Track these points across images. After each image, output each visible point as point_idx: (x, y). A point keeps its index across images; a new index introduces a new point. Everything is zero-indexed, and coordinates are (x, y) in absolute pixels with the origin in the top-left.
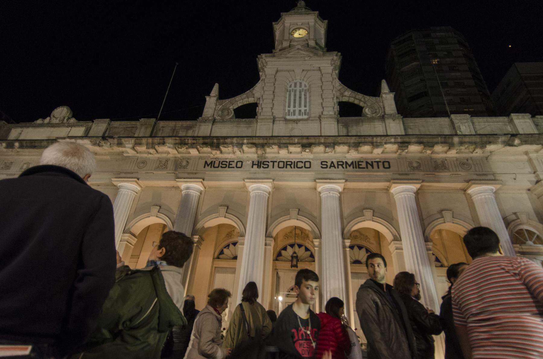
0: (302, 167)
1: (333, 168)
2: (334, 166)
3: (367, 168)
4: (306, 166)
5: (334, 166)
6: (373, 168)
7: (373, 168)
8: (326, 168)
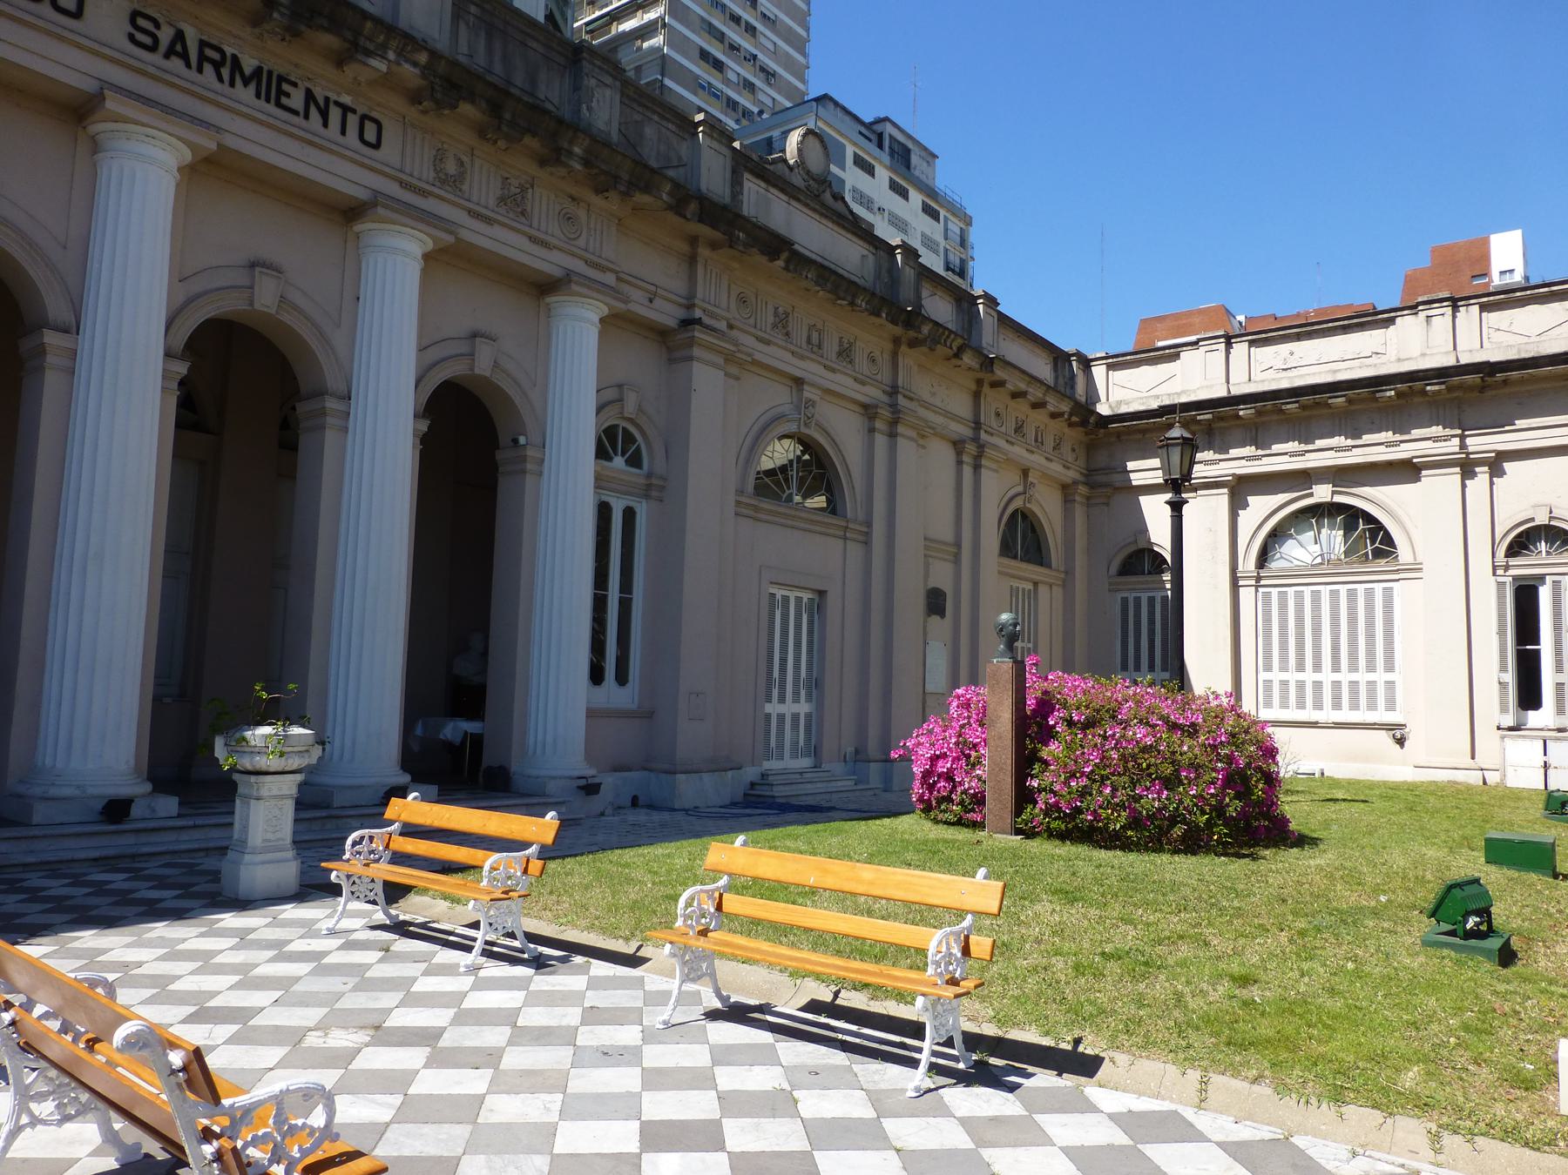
1: (176, 64)
2: (185, 57)
5: (185, 57)
6: (325, 125)
7: (325, 125)
8: (152, 49)
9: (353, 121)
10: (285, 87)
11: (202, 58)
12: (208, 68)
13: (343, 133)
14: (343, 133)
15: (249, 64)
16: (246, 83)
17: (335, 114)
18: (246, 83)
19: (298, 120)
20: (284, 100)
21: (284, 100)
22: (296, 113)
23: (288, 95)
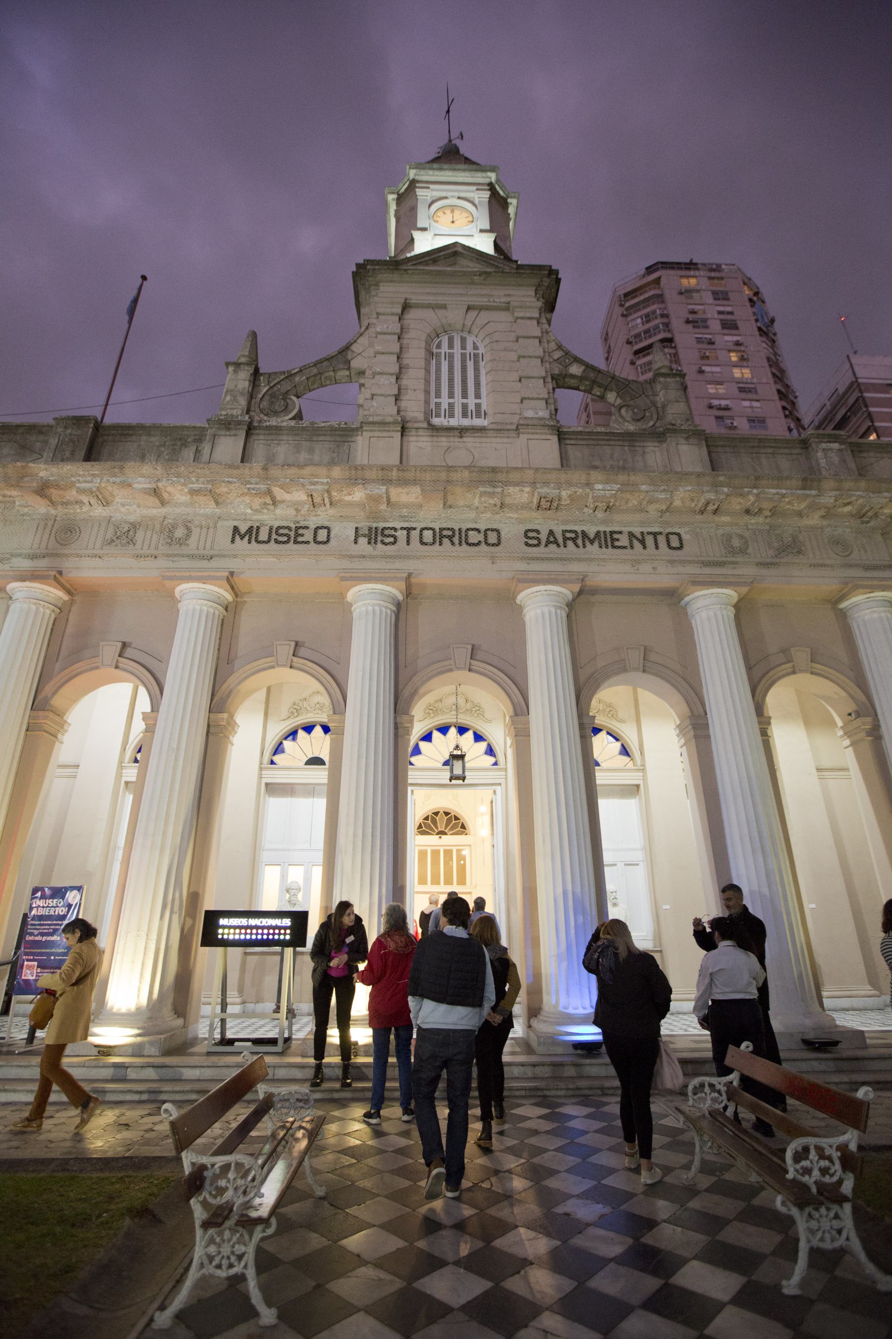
0: (479, 543)
3: (632, 547)
4: (319, 539)
6: (645, 547)
7: (645, 547)
8: (538, 545)
9: (661, 540)
10: (616, 536)
11: (565, 539)
12: (570, 544)
13: (657, 547)
14: (657, 547)
15: (592, 533)
16: (242, 537)
17: (649, 540)
18: (242, 537)
19: (629, 551)
20: (617, 544)
21: (617, 544)
22: (625, 547)
23: (302, 535)
